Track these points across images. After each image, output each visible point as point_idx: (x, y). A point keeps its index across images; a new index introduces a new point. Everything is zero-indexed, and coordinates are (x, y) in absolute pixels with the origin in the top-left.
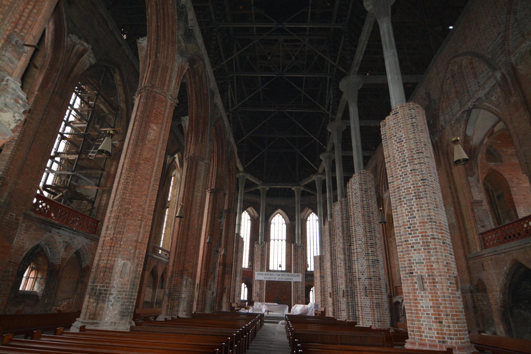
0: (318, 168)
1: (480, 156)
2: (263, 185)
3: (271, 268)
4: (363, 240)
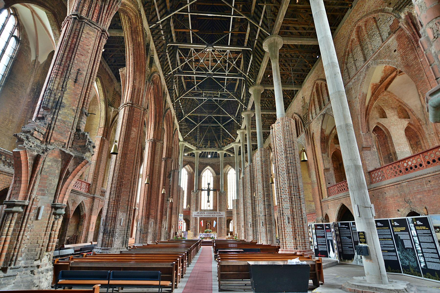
0: (236, 139)
1: (330, 141)
3: (202, 208)
4: (262, 192)
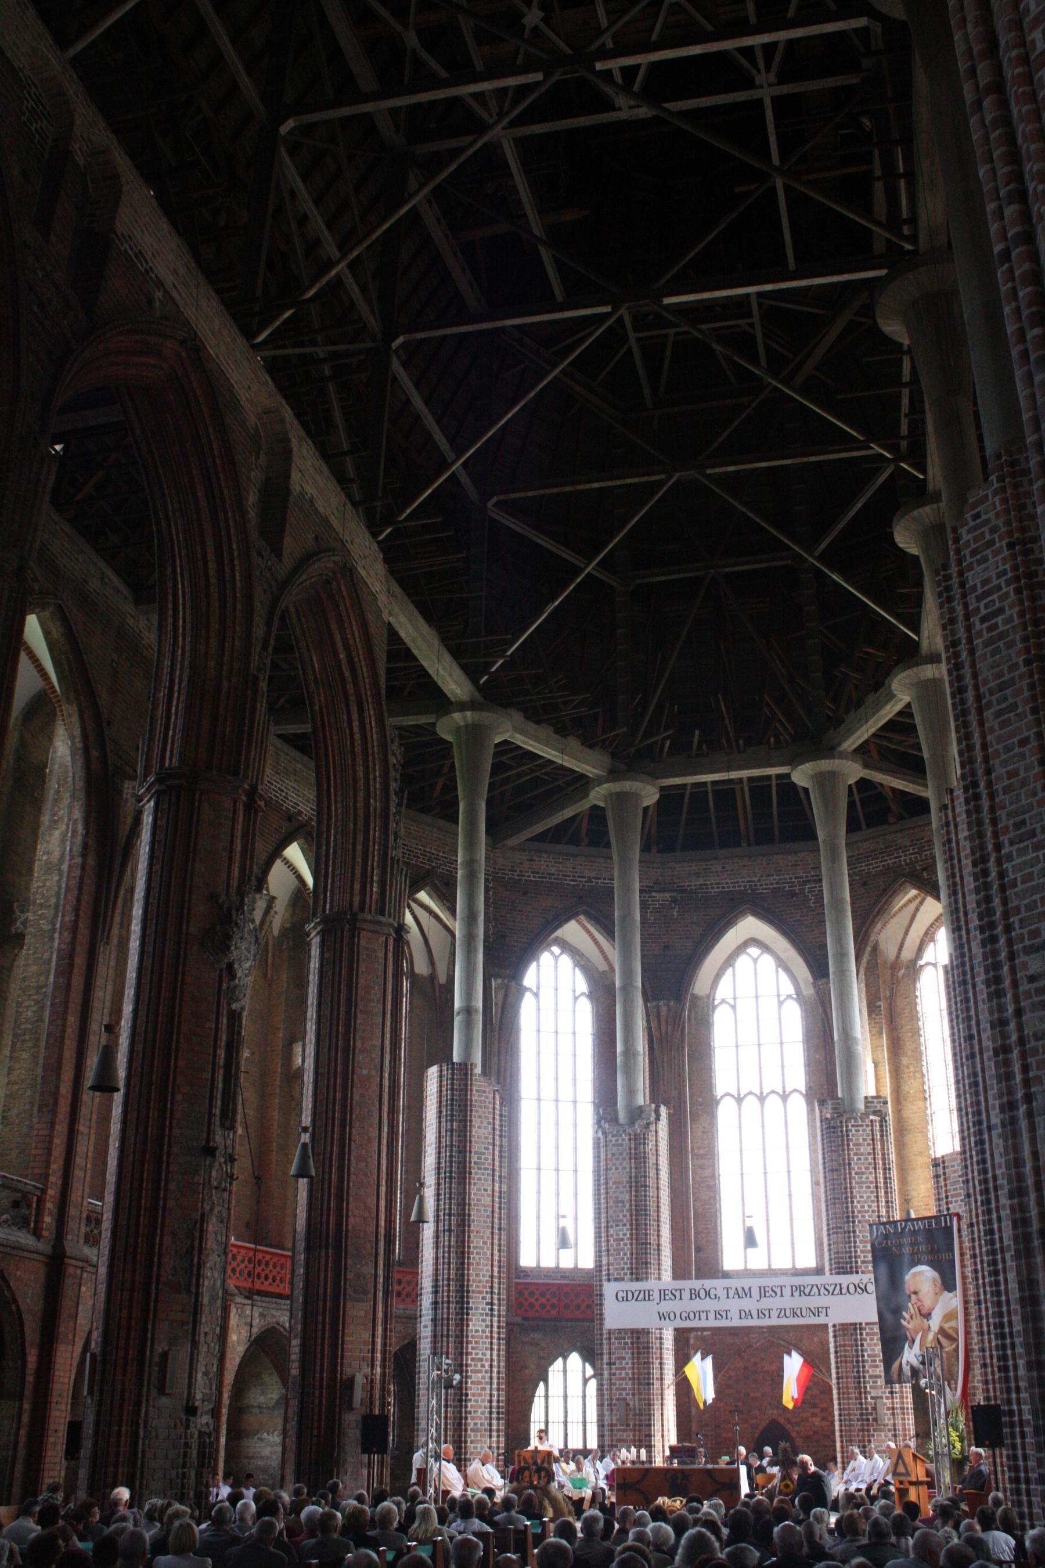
2: (614, 775)
